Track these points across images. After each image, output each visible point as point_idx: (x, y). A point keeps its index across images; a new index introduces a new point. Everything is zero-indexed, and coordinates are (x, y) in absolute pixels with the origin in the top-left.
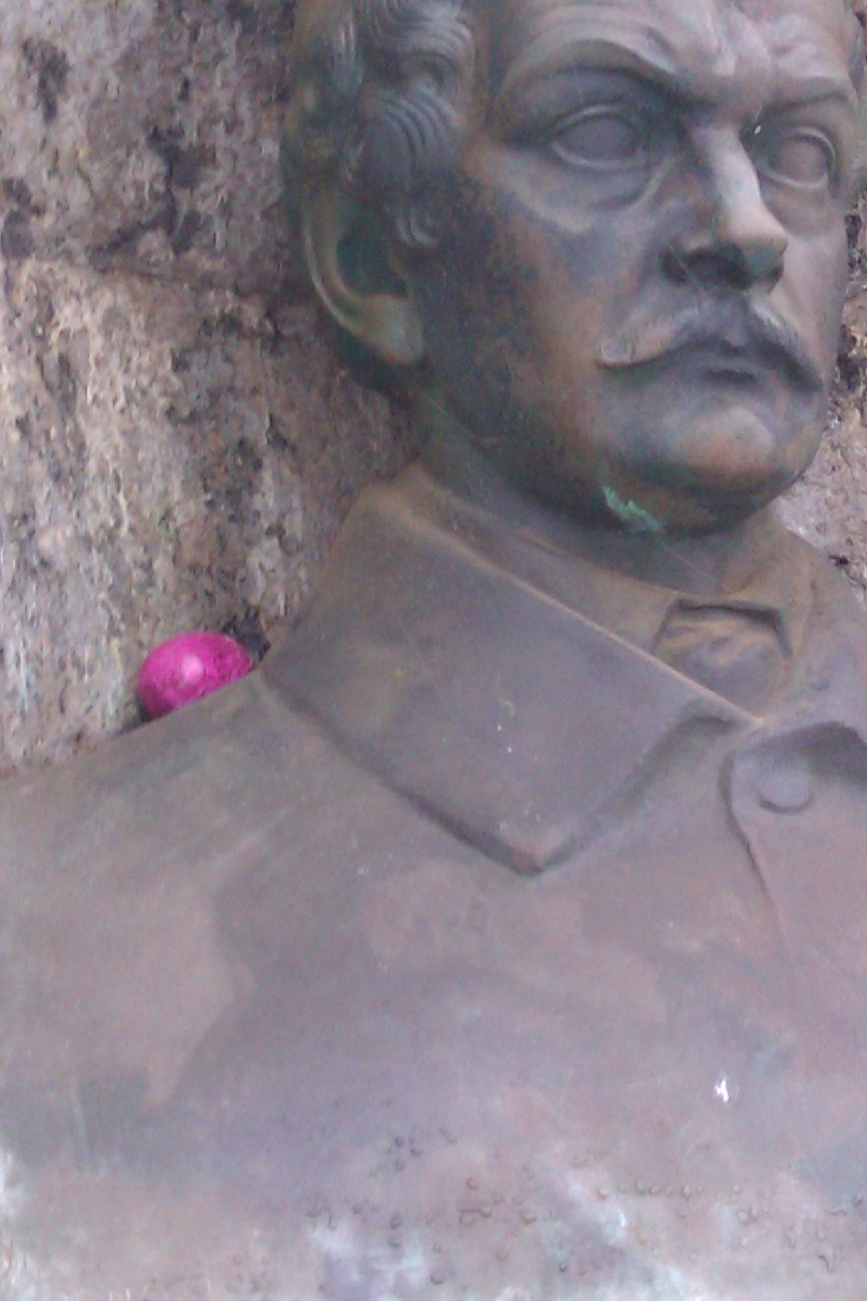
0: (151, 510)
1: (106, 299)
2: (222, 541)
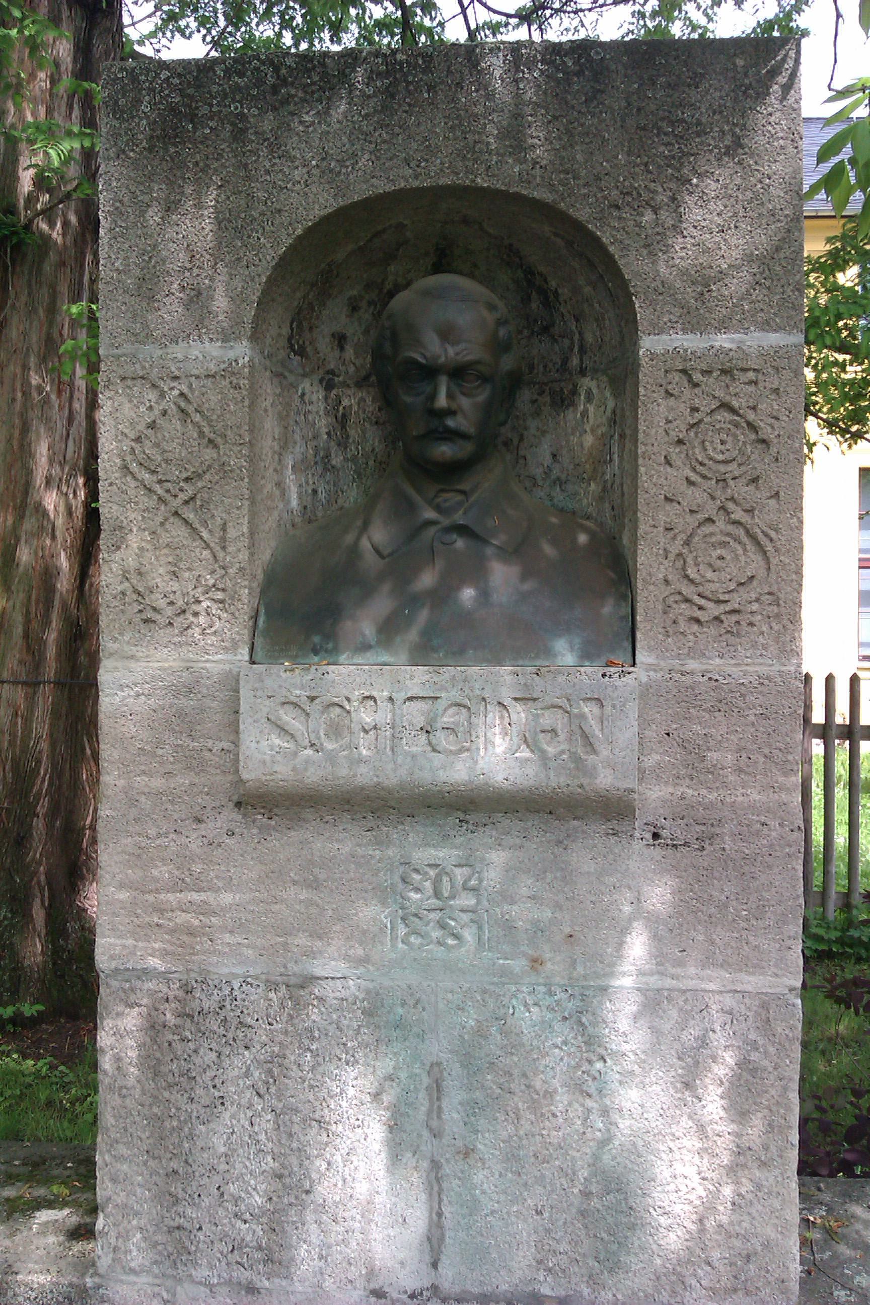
0: (368, 449)
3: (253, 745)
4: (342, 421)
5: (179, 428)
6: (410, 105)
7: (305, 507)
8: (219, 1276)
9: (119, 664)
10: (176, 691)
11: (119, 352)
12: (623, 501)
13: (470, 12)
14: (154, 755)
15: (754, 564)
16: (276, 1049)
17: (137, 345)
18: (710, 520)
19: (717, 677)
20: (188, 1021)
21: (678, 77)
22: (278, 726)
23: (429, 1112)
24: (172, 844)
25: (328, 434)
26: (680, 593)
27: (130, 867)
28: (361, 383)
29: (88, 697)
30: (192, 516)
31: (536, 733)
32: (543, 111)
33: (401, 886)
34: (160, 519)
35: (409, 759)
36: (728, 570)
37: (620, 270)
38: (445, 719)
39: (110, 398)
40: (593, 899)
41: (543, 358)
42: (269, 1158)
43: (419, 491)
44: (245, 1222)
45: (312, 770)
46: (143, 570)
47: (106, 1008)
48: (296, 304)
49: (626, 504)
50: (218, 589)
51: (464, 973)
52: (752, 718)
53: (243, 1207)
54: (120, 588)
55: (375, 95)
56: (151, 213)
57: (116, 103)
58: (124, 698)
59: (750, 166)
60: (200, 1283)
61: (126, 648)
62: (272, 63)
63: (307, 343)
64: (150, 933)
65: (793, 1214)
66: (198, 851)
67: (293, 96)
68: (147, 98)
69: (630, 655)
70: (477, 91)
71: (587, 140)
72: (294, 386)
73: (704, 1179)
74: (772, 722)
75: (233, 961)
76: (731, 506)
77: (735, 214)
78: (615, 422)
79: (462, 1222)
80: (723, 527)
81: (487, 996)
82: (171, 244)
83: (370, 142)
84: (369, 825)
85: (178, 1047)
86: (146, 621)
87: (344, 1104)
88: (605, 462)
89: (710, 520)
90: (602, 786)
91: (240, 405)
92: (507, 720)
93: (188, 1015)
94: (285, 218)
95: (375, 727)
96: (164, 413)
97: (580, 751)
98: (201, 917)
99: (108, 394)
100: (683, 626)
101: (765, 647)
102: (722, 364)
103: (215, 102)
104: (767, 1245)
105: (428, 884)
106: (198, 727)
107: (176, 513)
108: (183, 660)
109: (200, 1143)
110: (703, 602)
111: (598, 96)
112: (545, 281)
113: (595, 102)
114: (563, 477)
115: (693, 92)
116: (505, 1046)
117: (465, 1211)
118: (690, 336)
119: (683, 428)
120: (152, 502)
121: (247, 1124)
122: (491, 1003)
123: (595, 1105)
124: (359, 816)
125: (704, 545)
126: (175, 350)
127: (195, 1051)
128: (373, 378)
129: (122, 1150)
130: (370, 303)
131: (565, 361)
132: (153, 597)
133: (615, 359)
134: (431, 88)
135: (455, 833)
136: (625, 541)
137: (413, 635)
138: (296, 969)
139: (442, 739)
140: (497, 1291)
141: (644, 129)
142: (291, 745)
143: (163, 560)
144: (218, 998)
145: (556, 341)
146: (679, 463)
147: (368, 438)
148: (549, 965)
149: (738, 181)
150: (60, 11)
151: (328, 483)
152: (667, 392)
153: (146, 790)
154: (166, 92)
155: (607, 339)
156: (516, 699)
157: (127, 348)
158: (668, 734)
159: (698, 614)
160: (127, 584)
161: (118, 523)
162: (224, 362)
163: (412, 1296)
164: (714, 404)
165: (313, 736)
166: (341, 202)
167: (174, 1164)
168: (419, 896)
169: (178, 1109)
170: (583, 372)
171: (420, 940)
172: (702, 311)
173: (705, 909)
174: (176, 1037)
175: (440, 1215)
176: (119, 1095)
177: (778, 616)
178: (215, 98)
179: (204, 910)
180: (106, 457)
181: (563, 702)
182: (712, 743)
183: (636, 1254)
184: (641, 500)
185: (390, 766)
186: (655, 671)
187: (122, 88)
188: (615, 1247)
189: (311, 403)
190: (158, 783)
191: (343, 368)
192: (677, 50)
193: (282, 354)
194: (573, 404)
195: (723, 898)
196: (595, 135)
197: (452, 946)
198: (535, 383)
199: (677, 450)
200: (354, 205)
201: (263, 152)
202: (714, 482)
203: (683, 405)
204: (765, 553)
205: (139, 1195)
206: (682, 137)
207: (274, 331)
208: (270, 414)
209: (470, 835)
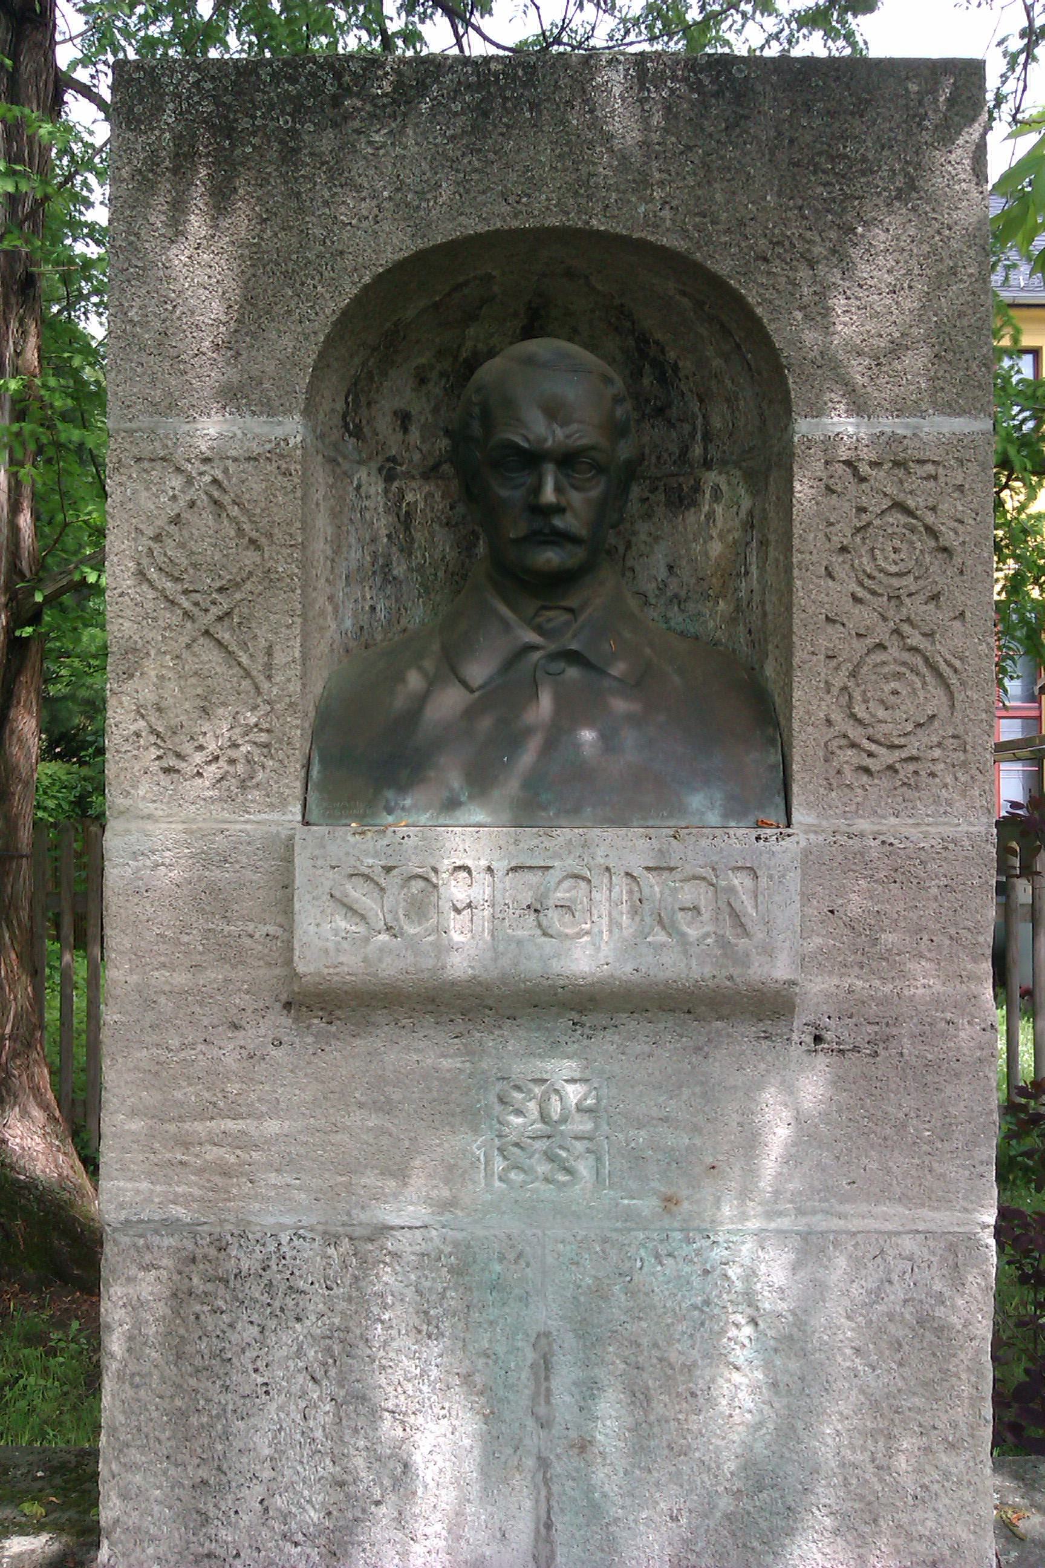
0: (438, 555)
1: (426, 489)
2: (463, 564)
3: (312, 929)
4: (406, 520)
5: (211, 523)
6: (507, 126)
7: (362, 628)
11: (134, 425)
13: (464, 40)
14: (178, 943)
15: (936, 700)
16: (337, 1321)
17: (156, 418)
18: (881, 646)
19: (892, 840)
20: (222, 1286)
22: (344, 905)
24: (201, 1057)
25: (389, 536)
26: (845, 736)
27: (146, 1089)
28: (430, 473)
30: (227, 636)
32: (673, 139)
33: (498, 1108)
34: (186, 639)
35: (514, 945)
36: (903, 707)
38: (559, 895)
39: (121, 484)
41: (657, 446)
42: (328, 1461)
44: (296, 1544)
46: (164, 704)
47: (113, 1271)
48: (353, 372)
49: (771, 626)
50: (261, 730)
51: (579, 1217)
52: (934, 891)
53: (294, 1526)
54: (133, 728)
55: (463, 112)
56: (175, 251)
57: (131, 110)
58: (139, 869)
59: (926, 213)
62: (332, 67)
63: (364, 422)
64: (171, 1173)
66: (234, 1066)
68: (171, 106)
71: (729, 176)
74: (959, 896)
75: (278, 1209)
76: (906, 628)
77: (909, 272)
78: (752, 526)
79: (577, 1535)
80: (896, 654)
81: (607, 1245)
82: (201, 291)
83: (458, 171)
84: (458, 1030)
85: (209, 1321)
86: (167, 771)
87: (425, 1389)
88: (738, 575)
89: (881, 646)
90: (756, 978)
91: (291, 496)
92: (637, 896)
93: (220, 1280)
94: (349, 262)
95: (469, 905)
96: (192, 504)
97: (729, 933)
98: (238, 1152)
99: (117, 478)
100: (849, 775)
102: (895, 454)
103: (259, 114)
105: (532, 1105)
106: (236, 907)
108: (216, 821)
109: (238, 1444)
111: (742, 123)
113: (738, 130)
115: (857, 122)
116: (631, 1309)
117: (581, 1520)
120: (175, 618)
121: (298, 1418)
122: (613, 1253)
123: (745, 1381)
125: (874, 677)
126: (206, 426)
127: (231, 1326)
129: (134, 1455)
130: (442, 374)
131: (685, 450)
132: (176, 739)
133: (751, 449)
135: (566, 1038)
136: (770, 670)
137: (512, 786)
138: (362, 1216)
139: (554, 919)
141: (797, 165)
142: (361, 929)
144: (260, 1257)
145: (673, 426)
147: (437, 545)
149: (912, 232)
151: (388, 597)
153: (167, 988)
154: (196, 99)
155: (741, 423)
156: (648, 869)
157: (144, 421)
158: (832, 912)
159: (868, 762)
160: (142, 723)
161: (131, 643)
162: (270, 441)
164: (886, 503)
165: (389, 917)
167: (203, 1473)
168: (520, 1120)
169: (208, 1401)
170: (707, 464)
172: (869, 389)
174: (206, 1308)
175: (549, 1526)
176: (131, 1384)
177: (964, 764)
178: (260, 109)
179: (241, 1142)
180: (115, 559)
181: (707, 872)
182: (887, 922)
184: (796, 621)
186: (816, 832)
187: (139, 91)
189: (368, 497)
190: (181, 979)
192: (837, 70)
193: (335, 435)
194: (694, 503)
195: (901, 1115)
196: (737, 171)
197: (564, 1184)
198: (645, 479)
199: (840, 559)
201: (321, 178)
202: (885, 598)
203: (847, 504)
204: (947, 687)
205: (156, 1515)
206: (843, 177)
207: (326, 406)
208: (322, 508)
209: (586, 1042)
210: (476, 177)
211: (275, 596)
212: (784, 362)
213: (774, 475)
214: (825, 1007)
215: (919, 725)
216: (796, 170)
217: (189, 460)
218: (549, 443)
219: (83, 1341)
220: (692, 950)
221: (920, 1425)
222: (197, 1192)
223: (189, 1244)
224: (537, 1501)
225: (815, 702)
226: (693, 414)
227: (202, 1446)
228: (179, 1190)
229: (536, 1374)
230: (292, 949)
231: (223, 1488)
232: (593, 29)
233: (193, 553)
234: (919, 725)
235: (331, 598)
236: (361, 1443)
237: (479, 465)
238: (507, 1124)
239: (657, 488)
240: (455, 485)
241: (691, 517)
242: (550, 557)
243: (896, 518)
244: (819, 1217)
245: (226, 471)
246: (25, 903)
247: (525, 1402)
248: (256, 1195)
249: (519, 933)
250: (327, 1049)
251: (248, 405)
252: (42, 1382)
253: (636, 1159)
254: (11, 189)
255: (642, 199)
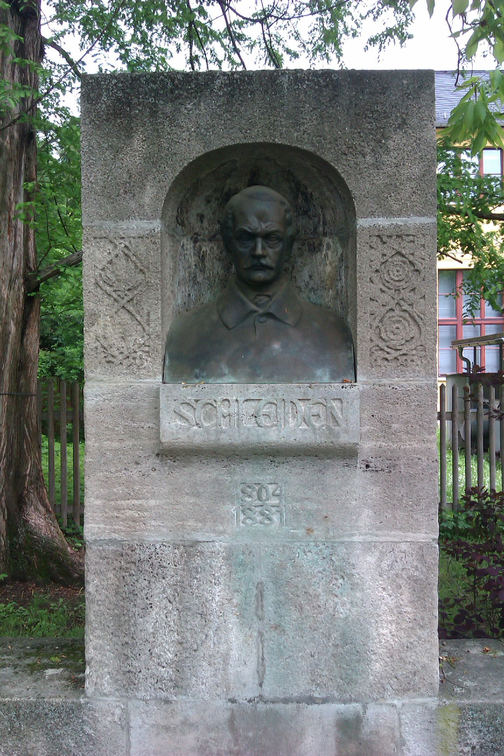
0: (215, 273)
1: (210, 245)
3: (167, 425)
4: (202, 258)
5: (124, 263)
6: (241, 100)
8: (150, 695)
9: (95, 384)
10: (125, 398)
11: (93, 224)
12: (347, 300)
13: (227, 13)
15: (414, 331)
16: (179, 578)
17: (102, 221)
18: (392, 310)
19: (396, 387)
21: (375, 89)
23: (257, 608)
26: (378, 346)
27: (102, 488)
28: (212, 238)
29: (26, 403)
30: (131, 308)
31: (309, 416)
32: (308, 105)
33: (241, 495)
35: (246, 430)
37: (347, 186)
40: (337, 498)
42: (176, 634)
43: (246, 296)
44: (163, 667)
45: (197, 436)
48: (180, 199)
49: (349, 301)
51: (274, 537)
52: (413, 407)
53: (162, 660)
54: (94, 345)
57: (89, 95)
58: (98, 401)
60: (141, 699)
61: (98, 376)
65: (436, 651)
66: (137, 479)
67: (181, 95)
68: (105, 93)
69: (354, 377)
70: (275, 94)
71: (330, 120)
72: (179, 241)
73: (393, 635)
74: (423, 409)
75: (156, 534)
76: (402, 303)
78: (342, 260)
80: (398, 313)
85: (128, 579)
86: (108, 362)
87: (214, 605)
88: (337, 280)
89: (392, 310)
92: (295, 411)
93: (133, 562)
94: (178, 158)
95: (229, 415)
96: (117, 256)
98: (139, 512)
99: (86, 245)
100: (379, 362)
101: (419, 372)
102: (397, 233)
104: (424, 667)
105: (255, 493)
106: (136, 416)
107: (123, 307)
108: (128, 382)
109: (140, 628)
110: (389, 350)
112: (306, 188)
114: (315, 287)
115: (382, 97)
117: (275, 657)
118: (381, 219)
119: (379, 264)
120: (111, 301)
122: (287, 551)
123: (339, 601)
124: (220, 460)
125: (389, 322)
128: (218, 236)
130: (216, 199)
131: (316, 228)
132: (112, 350)
133: (342, 229)
134: (252, 93)
135: (267, 467)
136: (349, 320)
140: (292, 697)
143: (117, 331)
144: (148, 554)
145: (311, 218)
146: (377, 281)
147: (215, 268)
148: (316, 532)
150: (6, 18)
151: (195, 290)
152: (370, 246)
153: (110, 448)
154: (115, 91)
157: (97, 222)
159: (387, 356)
160: (98, 343)
163: (250, 701)
165: (197, 420)
166: (207, 150)
167: (126, 639)
168: (250, 499)
170: (325, 234)
171: (251, 522)
173: (391, 501)
174: (127, 574)
175: (263, 659)
177: (425, 356)
179: (141, 509)
181: (323, 401)
182: (394, 420)
183: (360, 675)
184: (358, 300)
185: (237, 434)
188: (350, 672)
190: (115, 445)
191: (202, 232)
192: (374, 75)
193: (173, 225)
194: (320, 250)
195: (400, 496)
197: (268, 524)
200: (213, 151)
201: (167, 123)
204: (419, 326)
207: (170, 214)
208: (168, 255)
209: (276, 468)
210: (229, 122)
211: (151, 292)
212: (353, 196)
213: (350, 240)
214: (370, 454)
215: (407, 341)
216: (357, 117)
217: (115, 238)
218: (259, 230)
219: (65, 607)
220: (317, 432)
221: (409, 619)
222: (123, 528)
223: (120, 549)
224: (258, 649)
225: (366, 332)
226: (319, 214)
227: (126, 629)
228: (116, 527)
229: (257, 599)
230: (159, 433)
231: (134, 645)
232: (288, 7)
233: (117, 275)
234: (407, 341)
235: (172, 292)
236: (189, 627)
237: (232, 238)
238: (245, 501)
239: (305, 244)
240: (222, 243)
241: (318, 256)
242: (260, 275)
243: (399, 258)
244: (369, 536)
245: (130, 242)
246: (34, 416)
247: (253, 610)
248: (146, 529)
249: (249, 425)
250: (173, 472)
251: (139, 216)
252: (48, 624)
253: (296, 514)
254: (23, 96)
255: (296, 130)
